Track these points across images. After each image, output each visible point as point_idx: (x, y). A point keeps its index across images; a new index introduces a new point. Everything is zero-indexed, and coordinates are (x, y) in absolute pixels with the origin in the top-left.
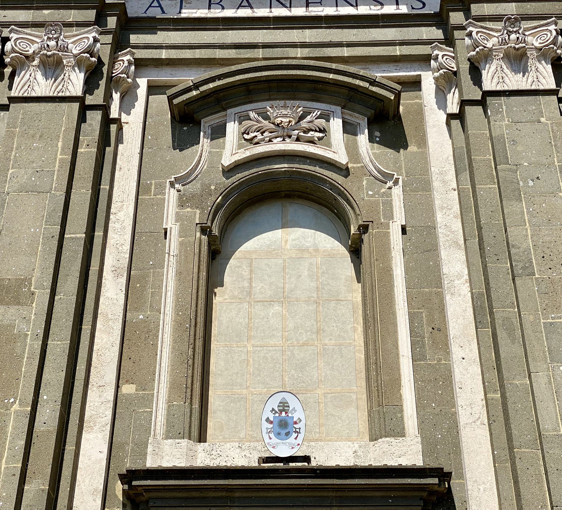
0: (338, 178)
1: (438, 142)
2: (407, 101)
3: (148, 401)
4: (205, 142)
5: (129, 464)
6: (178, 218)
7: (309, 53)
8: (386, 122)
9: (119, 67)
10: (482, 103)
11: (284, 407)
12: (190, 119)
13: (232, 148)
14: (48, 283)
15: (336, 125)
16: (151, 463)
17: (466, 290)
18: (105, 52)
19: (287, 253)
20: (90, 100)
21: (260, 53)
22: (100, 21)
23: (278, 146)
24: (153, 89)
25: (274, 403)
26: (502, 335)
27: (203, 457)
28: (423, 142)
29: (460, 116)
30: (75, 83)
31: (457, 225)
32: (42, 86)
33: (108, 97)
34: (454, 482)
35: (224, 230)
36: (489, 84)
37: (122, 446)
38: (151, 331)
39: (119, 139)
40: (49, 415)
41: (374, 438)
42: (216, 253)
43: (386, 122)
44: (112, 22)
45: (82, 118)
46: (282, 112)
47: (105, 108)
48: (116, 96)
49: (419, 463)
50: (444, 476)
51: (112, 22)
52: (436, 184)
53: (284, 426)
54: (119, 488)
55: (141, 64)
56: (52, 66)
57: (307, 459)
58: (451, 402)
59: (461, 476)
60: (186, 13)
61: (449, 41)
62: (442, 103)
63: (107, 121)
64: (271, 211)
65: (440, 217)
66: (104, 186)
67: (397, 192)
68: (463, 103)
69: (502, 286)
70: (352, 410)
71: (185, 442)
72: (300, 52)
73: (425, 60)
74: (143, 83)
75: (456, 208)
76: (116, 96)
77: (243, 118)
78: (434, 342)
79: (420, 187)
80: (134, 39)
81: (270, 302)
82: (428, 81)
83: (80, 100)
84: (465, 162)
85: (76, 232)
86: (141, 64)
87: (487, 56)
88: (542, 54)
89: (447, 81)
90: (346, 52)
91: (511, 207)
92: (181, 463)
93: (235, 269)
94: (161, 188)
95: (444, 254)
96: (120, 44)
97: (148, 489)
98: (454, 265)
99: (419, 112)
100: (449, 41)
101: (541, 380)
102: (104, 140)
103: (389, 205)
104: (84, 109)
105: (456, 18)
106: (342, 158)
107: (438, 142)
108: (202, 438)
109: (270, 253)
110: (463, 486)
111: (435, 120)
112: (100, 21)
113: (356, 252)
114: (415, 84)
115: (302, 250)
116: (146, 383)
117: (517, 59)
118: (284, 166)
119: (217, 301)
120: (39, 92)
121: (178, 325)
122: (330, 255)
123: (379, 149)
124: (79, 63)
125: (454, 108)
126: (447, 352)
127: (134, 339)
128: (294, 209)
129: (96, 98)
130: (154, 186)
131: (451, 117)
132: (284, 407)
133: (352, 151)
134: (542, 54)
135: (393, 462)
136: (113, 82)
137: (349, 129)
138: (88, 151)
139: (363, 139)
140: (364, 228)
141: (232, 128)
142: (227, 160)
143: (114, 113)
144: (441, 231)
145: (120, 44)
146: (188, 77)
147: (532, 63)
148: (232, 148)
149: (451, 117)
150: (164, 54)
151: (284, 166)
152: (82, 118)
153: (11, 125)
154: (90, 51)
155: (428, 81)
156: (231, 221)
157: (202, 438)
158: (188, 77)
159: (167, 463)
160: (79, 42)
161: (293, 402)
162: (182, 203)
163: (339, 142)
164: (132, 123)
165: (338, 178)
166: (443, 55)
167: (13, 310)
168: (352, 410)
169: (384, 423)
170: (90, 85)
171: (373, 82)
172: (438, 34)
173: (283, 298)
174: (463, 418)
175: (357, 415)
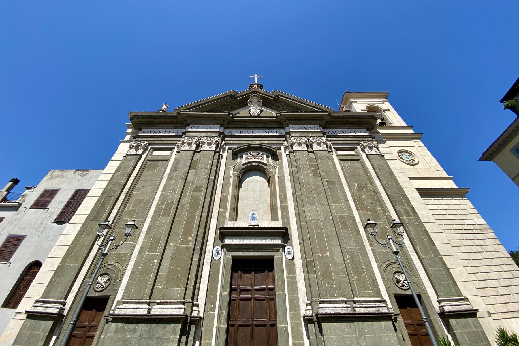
0: (265, 167)
1: (285, 160)
2: (278, 152)
3: (225, 212)
4: (239, 159)
5: (221, 226)
6: (233, 174)
7: (453, 308)
8: (275, 156)
9: (222, 144)
10: (293, 152)
11: (253, 214)
12: (236, 155)
13: (244, 160)
14: (206, 187)
15: (265, 156)
16: (225, 226)
17: (290, 189)
18: (220, 141)
19: (255, 183)
20: (216, 151)
21: (250, 142)
22: (219, 136)
23: (253, 160)
24: (229, 149)
25: (251, 213)
26: (298, 199)
27: (237, 225)
28: (282, 160)
29: (289, 155)
30: (214, 147)
31: (289, 176)
32: (187, 148)
33: (220, 150)
34: (289, 230)
35: (242, 177)
36: (294, 149)
37: (219, 222)
38: (226, 197)
39: (222, 158)
40: (204, 215)
41: (272, 221)
42: (240, 182)
43: (275, 156)
44: (221, 136)
45: (215, 154)
46: (254, 154)
47: (219, 152)
48: (222, 150)
49: (282, 226)
50: (287, 229)
51: (221, 136)
52: (284, 168)
53: (253, 218)
54: (218, 231)
55: (227, 144)
56: (209, 144)
57: (258, 225)
58: (288, 213)
59: (290, 229)
60: (236, 134)
61: (286, 140)
62: (285, 152)
63: (220, 155)
64: (252, 172)
65: (285, 175)
66: (218, 168)
67: (277, 169)
68: (289, 152)
69: (298, 189)
70: (267, 215)
71: (233, 221)
72: (258, 142)
73: (282, 144)
74: (227, 147)
75: (288, 173)
76: (222, 150)
77: (246, 154)
78: (285, 201)
79: (281, 168)
80: (226, 139)
81: (251, 192)
82: (283, 148)
83: (214, 151)
84: (290, 163)
85: (212, 177)
86: (227, 144)
87: (294, 143)
88: (304, 143)
89: (286, 148)
90: (267, 142)
91: (299, 173)
92: (232, 226)
93: (244, 184)
94: (230, 168)
95: (286, 182)
96: (223, 140)
97: (225, 232)
98: (288, 184)
99: (281, 153)
100: (286, 140)
101: (306, 208)
102: (219, 158)
103: (275, 172)
104: (215, 152)
105: (288, 136)
106: (266, 162)
107: (285, 160)
108: (236, 220)
109: (251, 181)
110: (290, 231)
111: (284, 155)
112: (219, 136)
113: (268, 181)
114: (280, 148)
115: (258, 181)
116: (225, 208)
117: (300, 144)
118: (254, 164)
119: (240, 191)
120: (186, 149)
121: (232, 196)
122: (263, 182)
123: (273, 161)
124: (215, 144)
125: (288, 153)
126: (287, 203)
127: (223, 199)
128: (256, 172)
129: (218, 150)
130: (227, 168)
131: (287, 155)
132: (253, 214)
133: (268, 161)
134: (304, 143)
135: (276, 226)
136: (221, 147)
137: (267, 157)
138: (215, 160)
139: (270, 159)
140: (270, 177)
141: (244, 156)
142: (243, 163)
143: (221, 153)
144: (285, 177)
145: (223, 140)
146: (236, 146)
147: (303, 145)
148: (244, 160)
149: (287, 155)
150: (231, 142)
151: (254, 164)
152: (215, 154)
153: (201, 155)
154: (217, 141)
155: (283, 148)
156: (297, 109)
157: (236, 220)
158: (236, 146)
159: (229, 226)
160: (215, 140)
161: (255, 213)
162: (234, 171)
163: (265, 159)
164: (225, 155)
165: (265, 167)
166: (286, 143)
167: (198, 193)
168: (267, 215)
169: (274, 218)
170: (217, 148)
171: (272, 148)
172: (284, 139)
173: (254, 191)
174: (291, 216)
175: (269, 216)
